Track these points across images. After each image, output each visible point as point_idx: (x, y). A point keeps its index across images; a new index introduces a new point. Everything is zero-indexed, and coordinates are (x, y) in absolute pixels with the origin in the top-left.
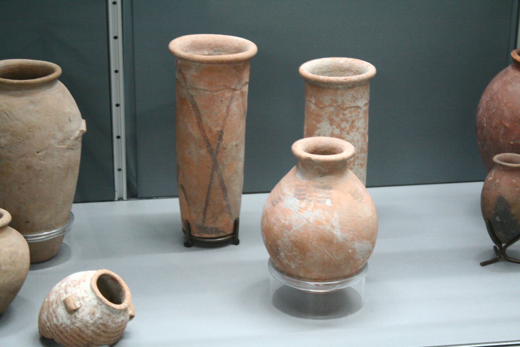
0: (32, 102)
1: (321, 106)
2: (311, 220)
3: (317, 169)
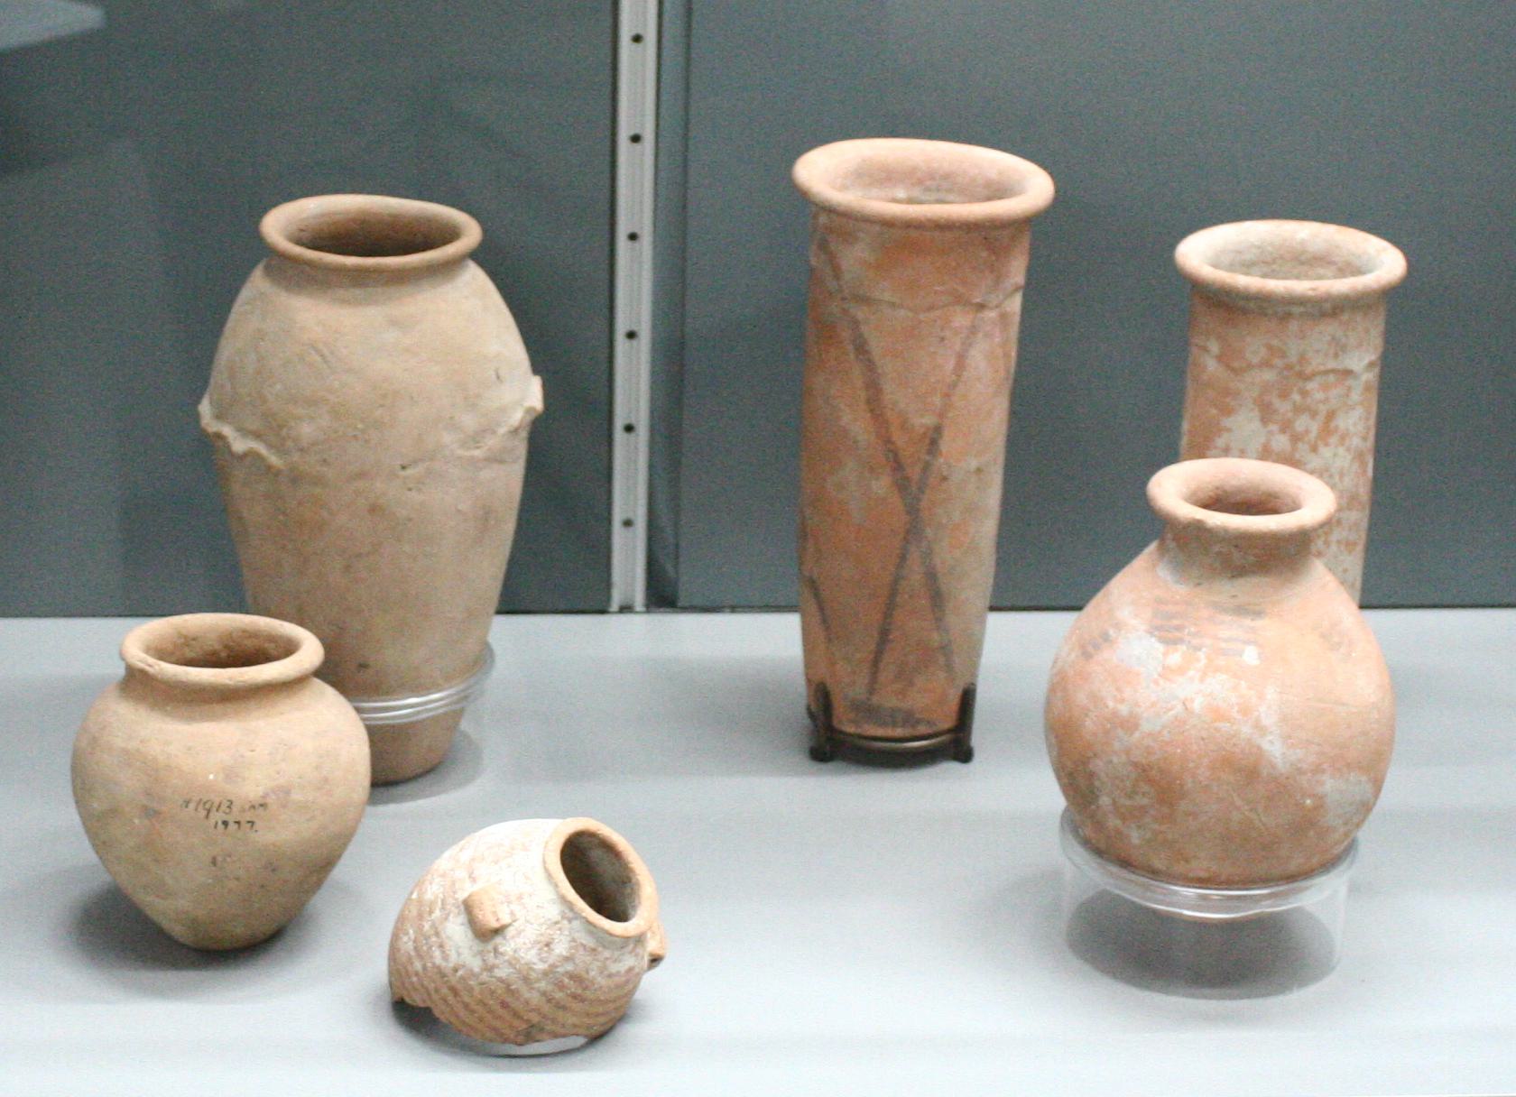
0: (394, 323)
1: (1236, 364)
2: (1197, 705)
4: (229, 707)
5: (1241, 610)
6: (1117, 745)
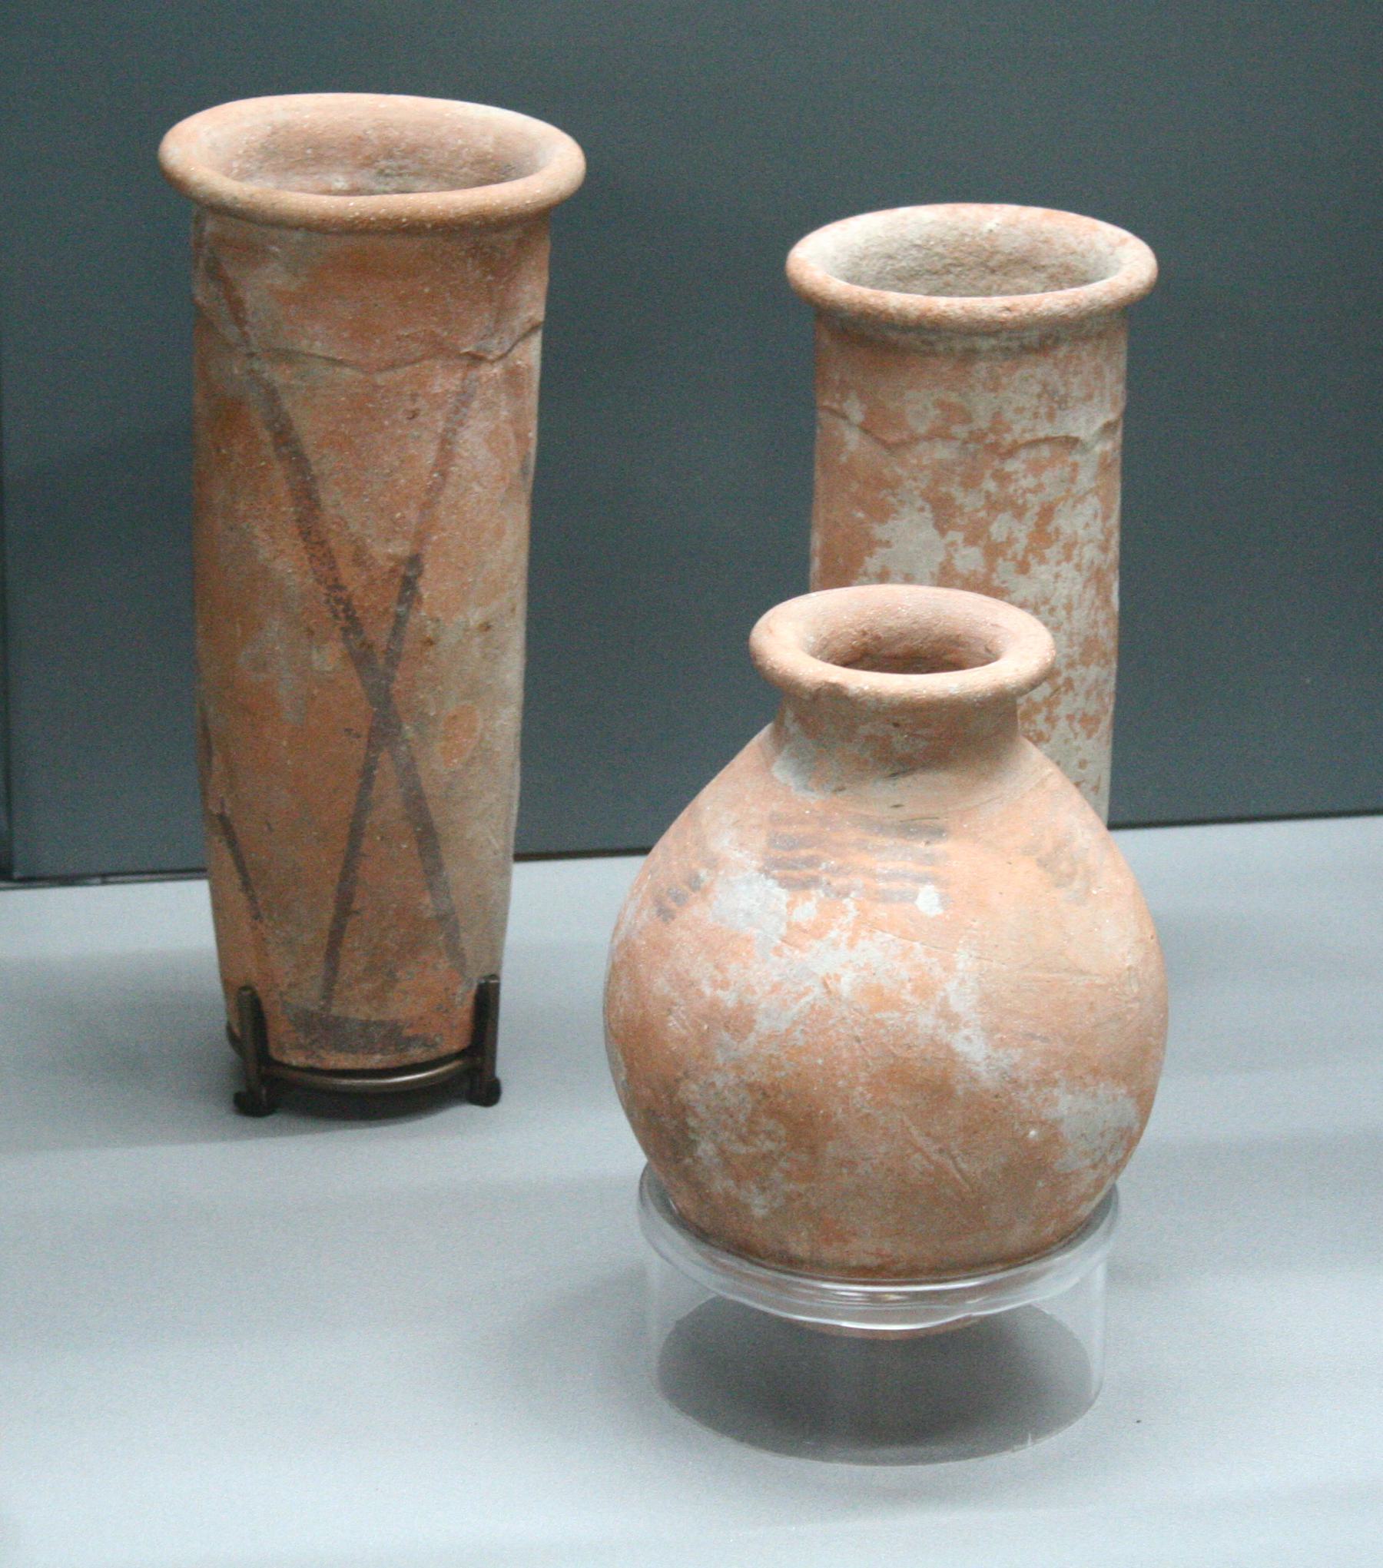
1: (892, 437)
2: (845, 986)
3: (870, 738)
6: (720, 1060)
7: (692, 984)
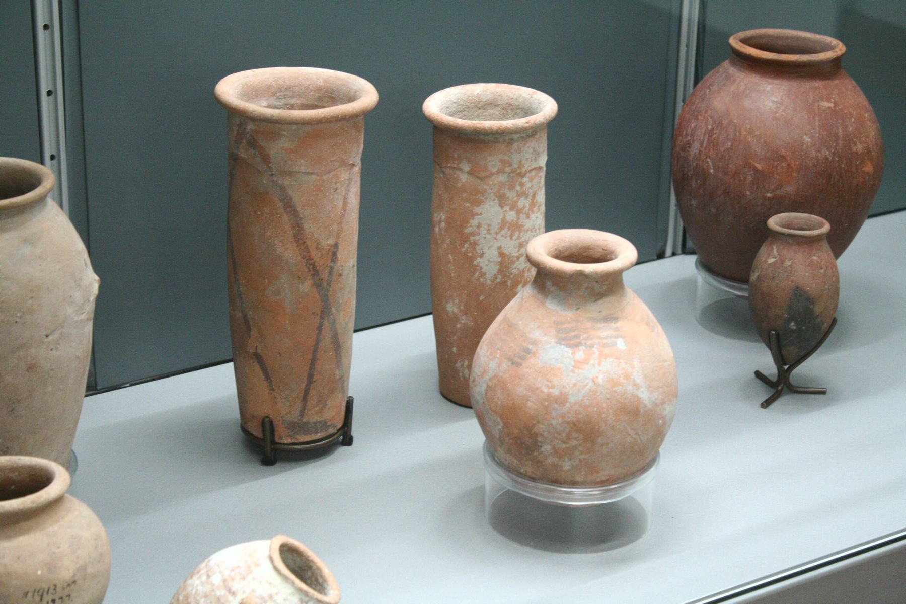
0: (26, 241)
1: (482, 174)
2: (601, 380)
3: (587, 288)
4: (31, 523)
5: (609, 318)
6: (554, 414)
7: (537, 388)
